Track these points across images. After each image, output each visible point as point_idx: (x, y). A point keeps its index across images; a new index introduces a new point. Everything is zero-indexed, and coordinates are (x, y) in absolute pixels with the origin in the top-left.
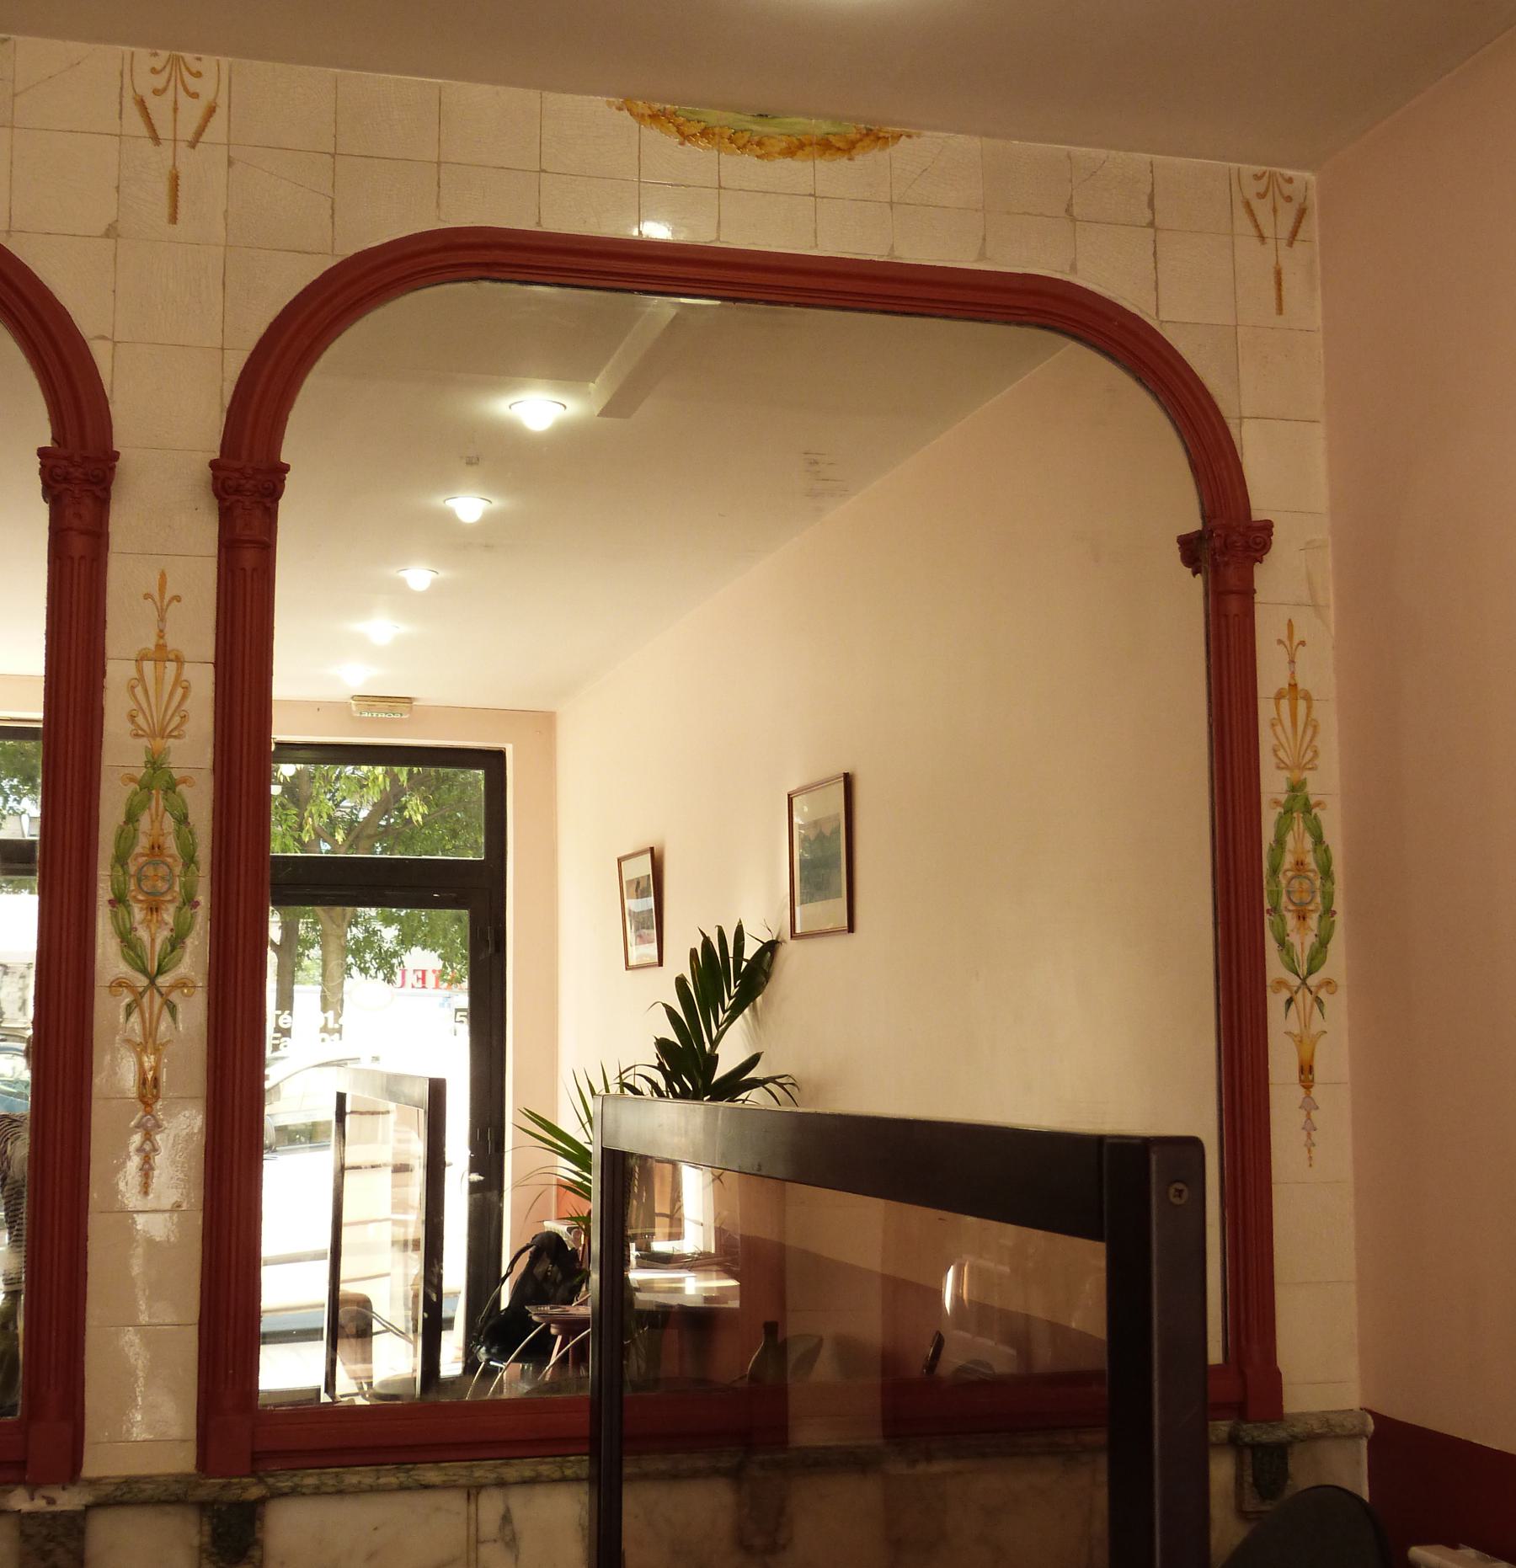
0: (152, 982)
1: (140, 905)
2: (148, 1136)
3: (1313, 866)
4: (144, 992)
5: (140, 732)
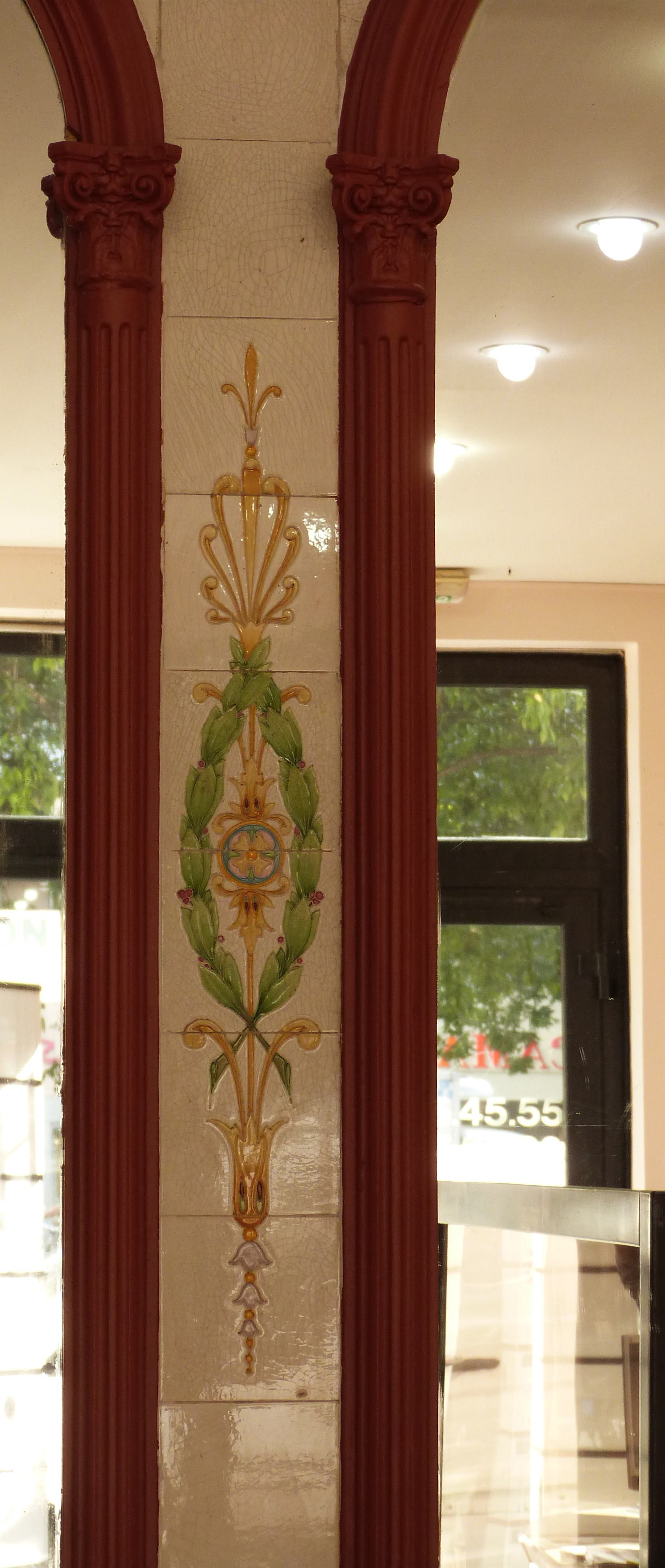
0: (251, 1025)
1: (230, 899)
2: (249, 1314)
5: (222, 614)
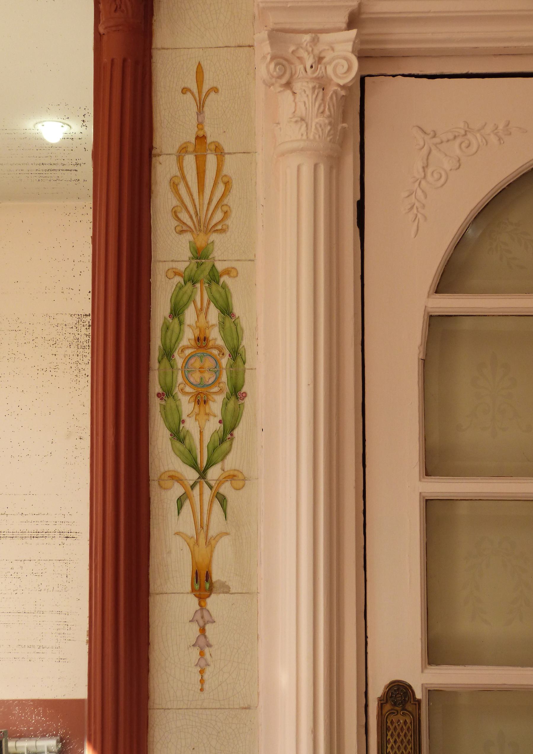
3: (220, 342)
4: (193, 487)
